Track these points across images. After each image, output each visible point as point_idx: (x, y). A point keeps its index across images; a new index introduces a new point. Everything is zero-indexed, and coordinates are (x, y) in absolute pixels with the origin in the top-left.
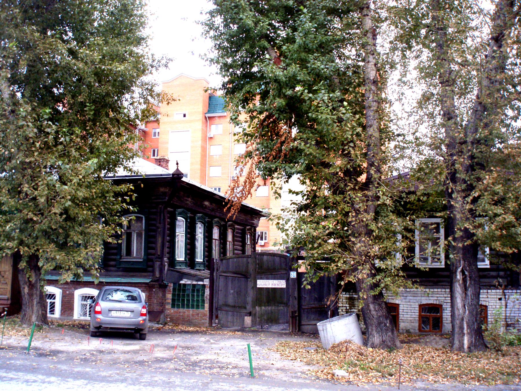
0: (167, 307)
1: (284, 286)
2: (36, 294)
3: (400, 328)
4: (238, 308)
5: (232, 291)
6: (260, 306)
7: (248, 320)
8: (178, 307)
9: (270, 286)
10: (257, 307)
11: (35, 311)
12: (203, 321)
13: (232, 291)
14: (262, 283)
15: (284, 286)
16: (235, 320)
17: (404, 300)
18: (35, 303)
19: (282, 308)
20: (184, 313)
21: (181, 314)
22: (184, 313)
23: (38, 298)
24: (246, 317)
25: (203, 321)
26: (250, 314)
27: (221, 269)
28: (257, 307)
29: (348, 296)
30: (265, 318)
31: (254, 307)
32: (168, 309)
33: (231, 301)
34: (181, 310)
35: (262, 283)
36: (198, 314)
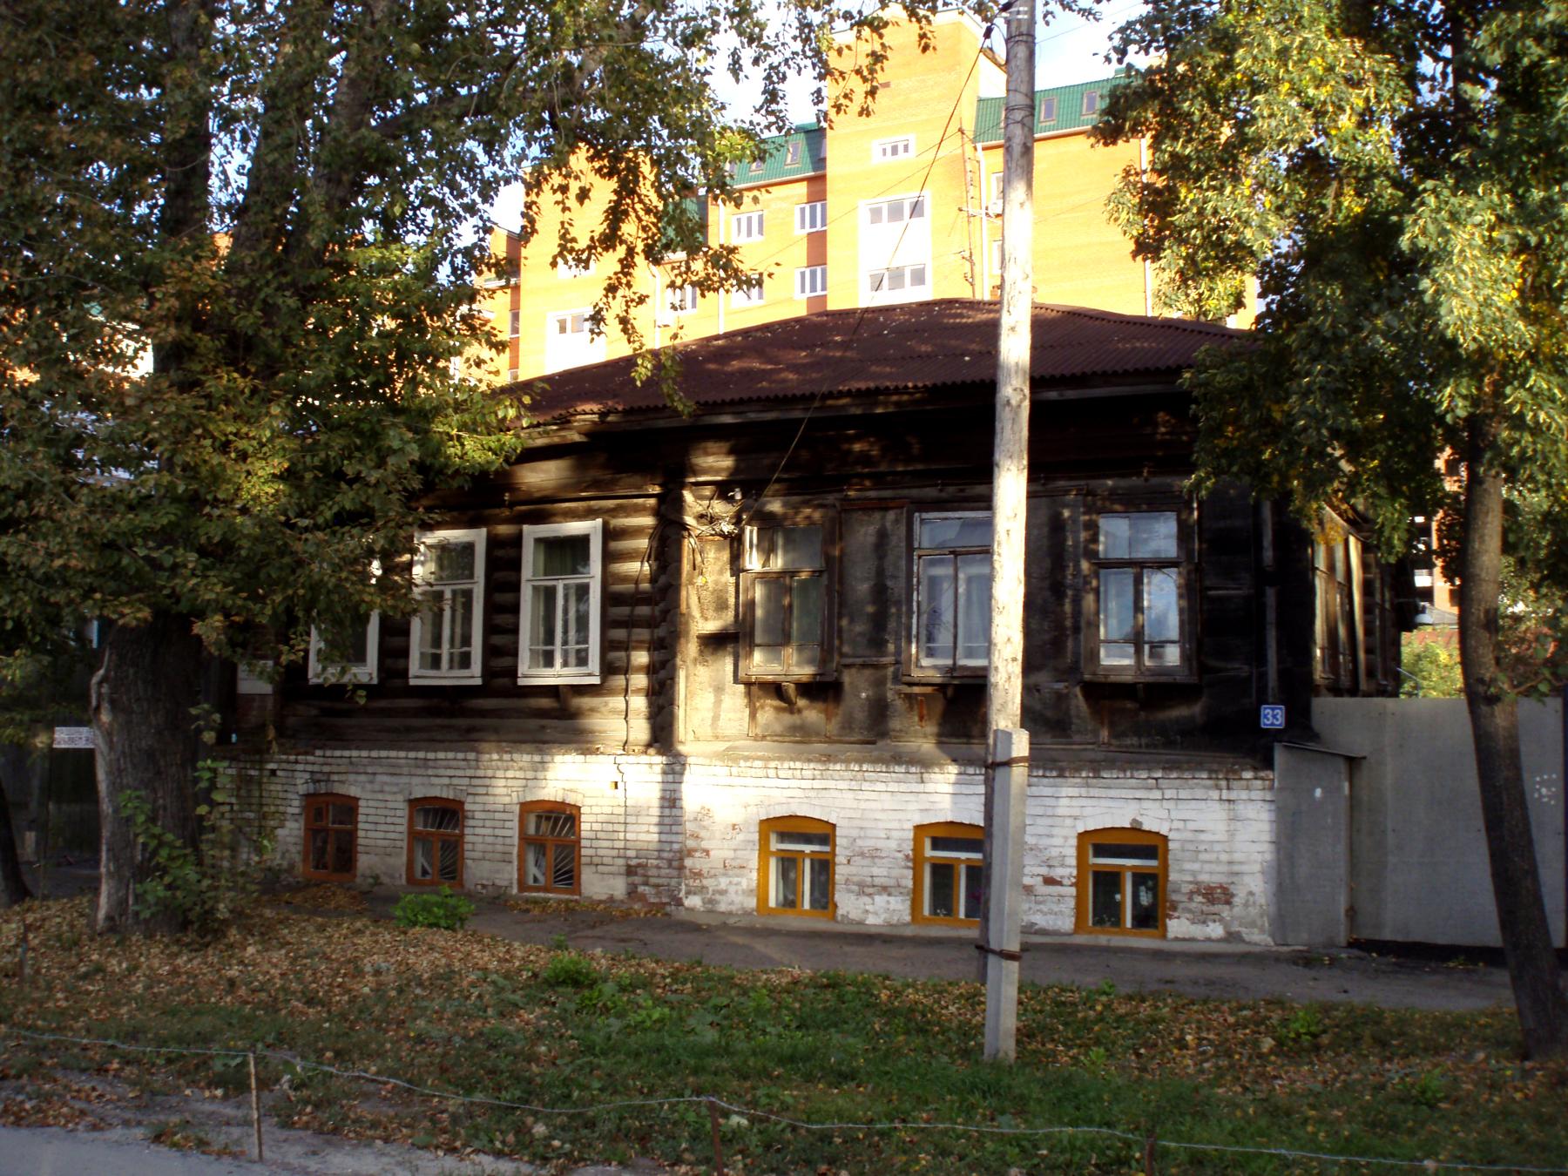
17: (368, 786)
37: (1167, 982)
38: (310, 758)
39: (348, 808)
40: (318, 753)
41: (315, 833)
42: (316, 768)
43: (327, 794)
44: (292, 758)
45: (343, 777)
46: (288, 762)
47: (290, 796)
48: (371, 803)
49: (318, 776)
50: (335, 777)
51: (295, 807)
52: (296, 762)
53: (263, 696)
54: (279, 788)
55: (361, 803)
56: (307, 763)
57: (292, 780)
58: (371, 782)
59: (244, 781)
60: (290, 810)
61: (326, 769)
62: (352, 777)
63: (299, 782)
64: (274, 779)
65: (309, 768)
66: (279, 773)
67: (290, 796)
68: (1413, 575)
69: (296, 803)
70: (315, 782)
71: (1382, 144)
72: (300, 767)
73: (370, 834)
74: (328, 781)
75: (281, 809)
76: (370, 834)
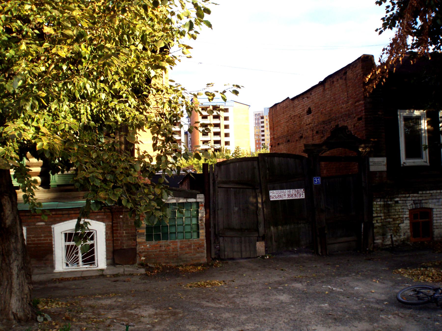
0: (138, 240)
1: (303, 196)
2: (16, 249)
3: (435, 236)
4: (248, 230)
5: (236, 209)
6: (276, 225)
7: (260, 246)
8: (158, 238)
9: (286, 198)
10: (272, 228)
11: (16, 287)
12: (198, 255)
13: (236, 209)
14: (276, 195)
15: (303, 196)
16: (243, 248)
17: (437, 204)
18: (15, 271)
19: (302, 225)
20: (168, 246)
21: (164, 249)
22: (168, 246)
23: (20, 258)
24: (258, 244)
25: (198, 255)
26: (263, 238)
27: (219, 179)
28: (272, 228)
29: (382, 203)
30: (284, 240)
31: (267, 226)
32: (141, 243)
33: (235, 221)
34: (163, 242)
35: (276, 195)
36: (189, 246)
37: (328, 264)
38: (415, 195)
39: (428, 213)
40: (420, 192)
41: (414, 226)
42: (416, 198)
43: (420, 208)
44: (408, 195)
45: (426, 201)
46: (405, 197)
47: (404, 210)
48: (438, 210)
49: (416, 202)
50: (423, 201)
51: (407, 215)
52: (409, 197)
53: (381, 172)
54: (400, 208)
55: (434, 210)
56: (413, 197)
57: (404, 206)
58: (438, 202)
59: (387, 207)
60: (405, 216)
61: (420, 198)
62: (430, 201)
63: (408, 204)
64: (397, 204)
65: (414, 199)
66: (399, 202)
67: (404, 210)
68: (387, 169)
69: (408, 213)
70: (415, 204)
71: (64, 110)
72: (410, 199)
73: (438, 221)
74: (406, 203)
75: (401, 216)
76: (438, 221)
